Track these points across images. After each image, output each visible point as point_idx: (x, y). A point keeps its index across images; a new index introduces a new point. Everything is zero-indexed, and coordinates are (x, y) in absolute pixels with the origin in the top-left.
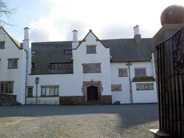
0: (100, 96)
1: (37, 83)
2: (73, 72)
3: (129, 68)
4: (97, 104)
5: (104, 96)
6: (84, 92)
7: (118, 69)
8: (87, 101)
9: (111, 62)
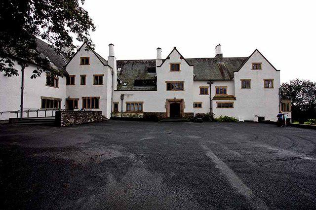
1: (122, 99)
3: (210, 87)
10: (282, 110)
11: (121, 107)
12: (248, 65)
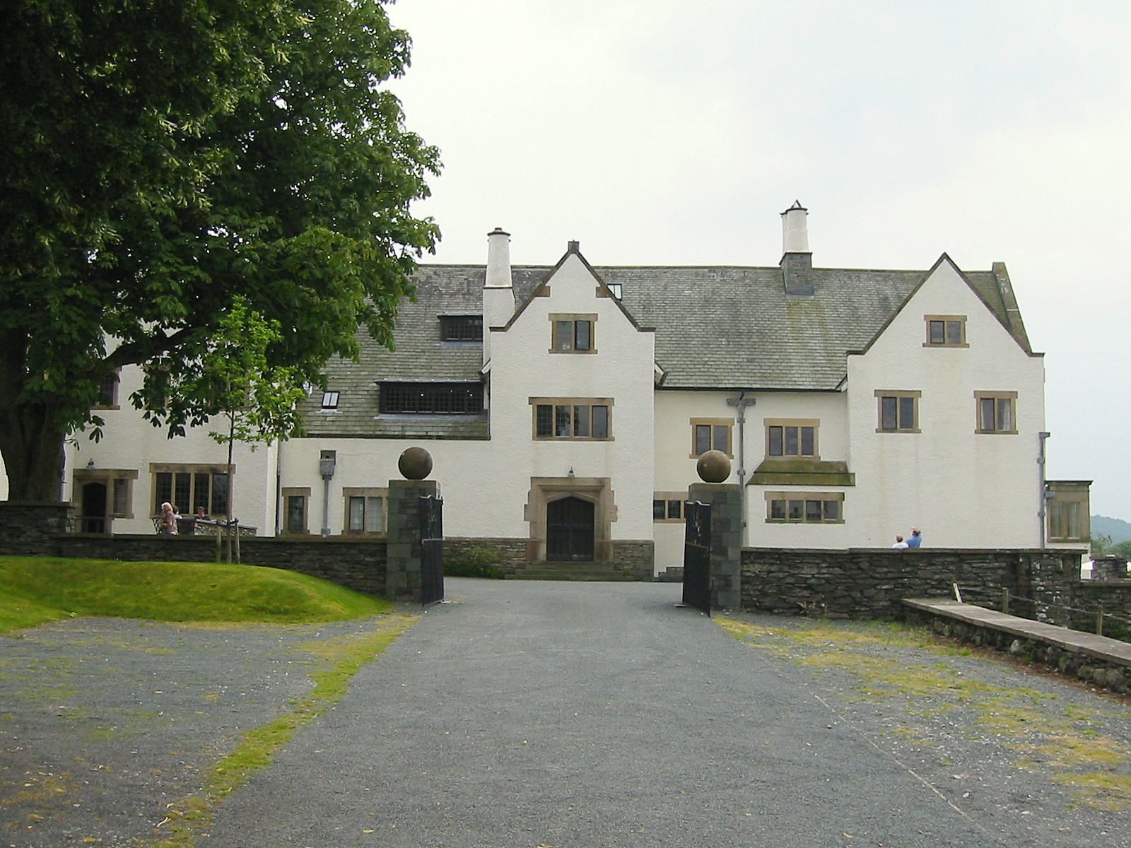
0: (606, 544)
1: (327, 477)
2: (487, 428)
3: (741, 421)
4: (587, 574)
5: (620, 545)
6: (534, 524)
7: (692, 421)
8: (544, 563)
9: (658, 387)
10: (1052, 533)
11: (331, 508)
12: (909, 326)
